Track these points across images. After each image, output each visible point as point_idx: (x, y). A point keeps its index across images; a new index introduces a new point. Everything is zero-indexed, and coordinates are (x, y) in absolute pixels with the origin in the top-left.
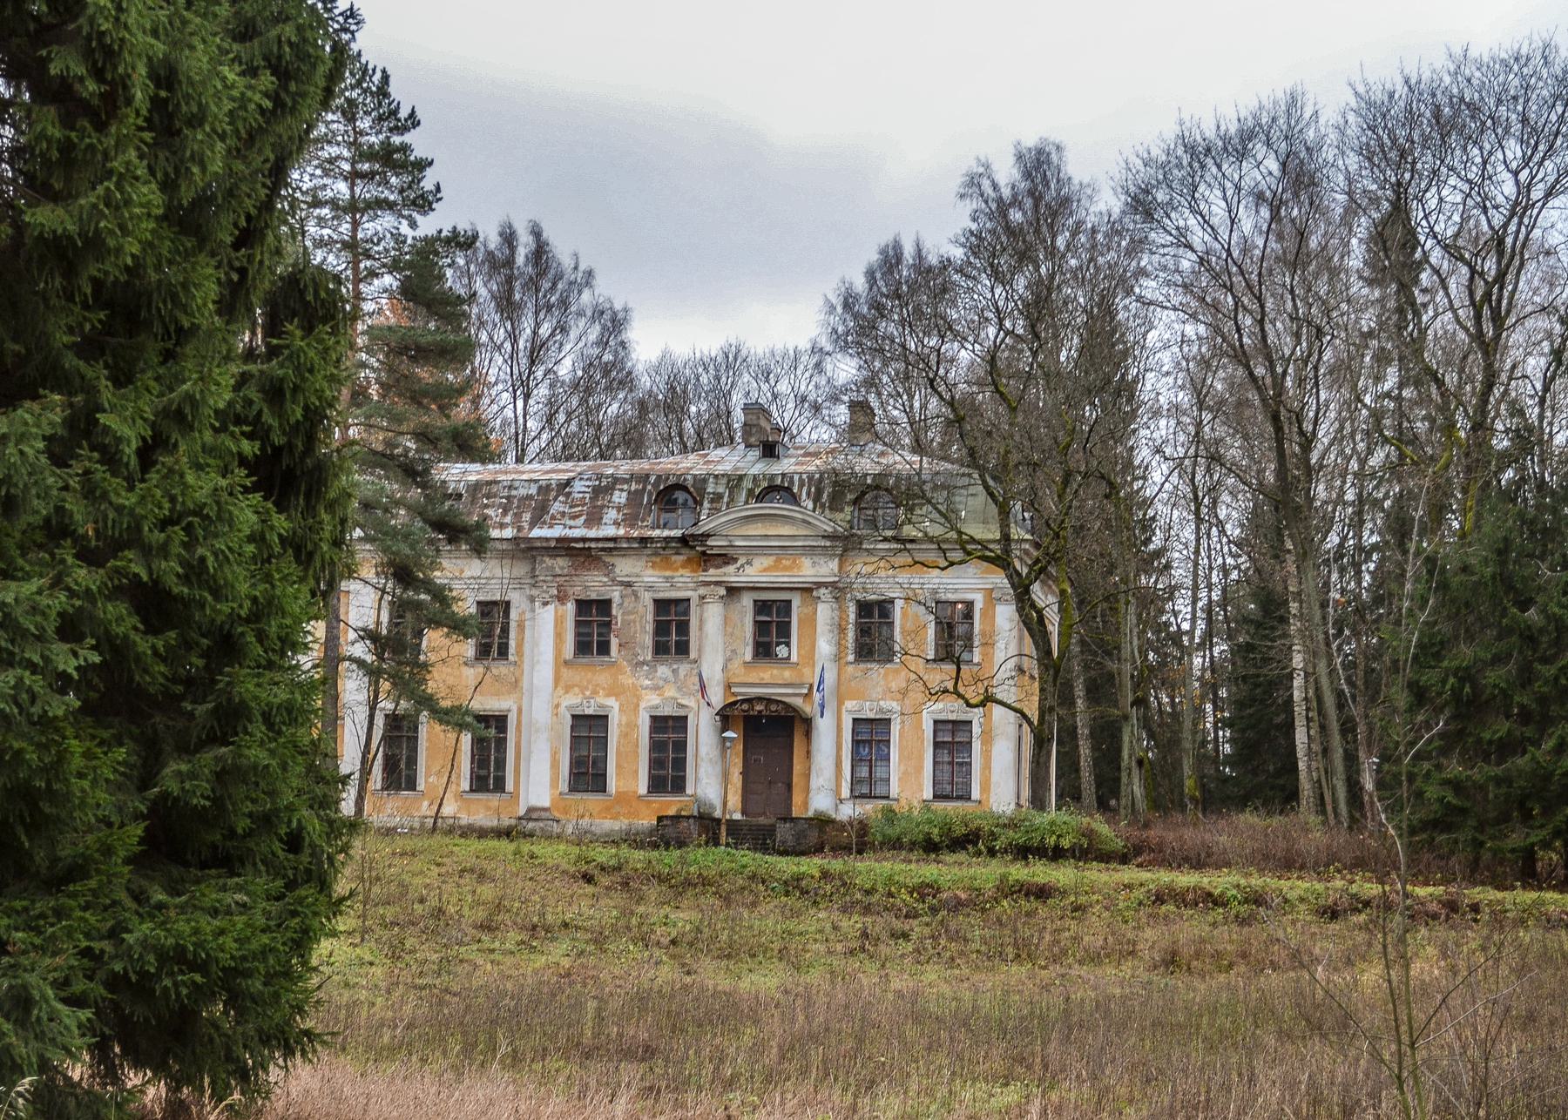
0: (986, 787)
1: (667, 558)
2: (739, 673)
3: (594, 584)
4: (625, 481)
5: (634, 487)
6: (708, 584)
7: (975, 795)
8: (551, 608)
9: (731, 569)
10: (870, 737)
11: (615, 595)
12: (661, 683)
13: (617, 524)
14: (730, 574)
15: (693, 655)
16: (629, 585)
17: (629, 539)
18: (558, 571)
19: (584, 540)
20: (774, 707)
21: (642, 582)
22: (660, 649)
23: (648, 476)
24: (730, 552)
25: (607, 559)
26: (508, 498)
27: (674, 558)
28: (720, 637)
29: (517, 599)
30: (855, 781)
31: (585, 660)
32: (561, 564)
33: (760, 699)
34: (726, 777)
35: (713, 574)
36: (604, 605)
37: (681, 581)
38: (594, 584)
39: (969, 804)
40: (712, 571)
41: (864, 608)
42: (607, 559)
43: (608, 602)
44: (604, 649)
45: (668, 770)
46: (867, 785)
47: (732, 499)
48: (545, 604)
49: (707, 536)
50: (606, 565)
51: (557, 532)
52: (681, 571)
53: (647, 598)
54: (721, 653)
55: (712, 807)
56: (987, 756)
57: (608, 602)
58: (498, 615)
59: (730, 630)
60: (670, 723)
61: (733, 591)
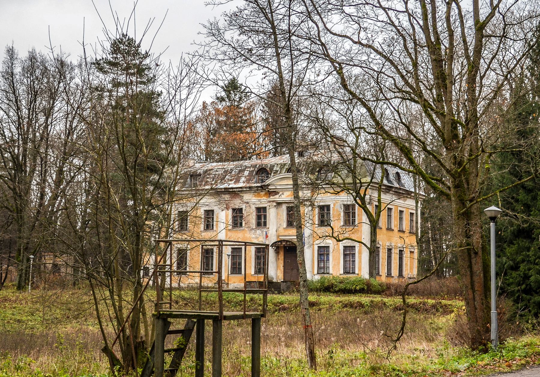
0: (360, 269)
1: (259, 193)
2: (282, 232)
3: (237, 203)
4: (249, 167)
5: (252, 169)
6: (270, 202)
7: (357, 272)
8: (224, 212)
9: (277, 196)
10: (323, 253)
11: (244, 207)
12: (258, 236)
13: (244, 182)
14: (277, 198)
15: (267, 227)
16: (247, 203)
17: (246, 187)
18: (226, 199)
19: (232, 188)
20: (288, 243)
21: (251, 202)
22: (259, 224)
23: (256, 165)
24: (277, 190)
25: (241, 194)
26: (215, 175)
27: (261, 193)
28: (277, 220)
29: (216, 209)
30: (319, 268)
31: (237, 229)
32: (227, 197)
33: (284, 241)
34: (278, 267)
35: (272, 198)
36: (241, 210)
37: (263, 201)
38: (237, 203)
39: (354, 275)
40: (271, 197)
41: (322, 208)
42: (241, 194)
43: (242, 209)
44: (241, 224)
45: (261, 266)
46: (322, 269)
47: (280, 172)
48: (223, 210)
49: (269, 185)
50: (241, 196)
51: (226, 186)
52: (264, 198)
53: (253, 208)
54: (275, 225)
55: (273, 278)
56: (360, 258)
57: (242, 209)
58: (211, 213)
59: (279, 217)
60: (262, 250)
61: (279, 204)
